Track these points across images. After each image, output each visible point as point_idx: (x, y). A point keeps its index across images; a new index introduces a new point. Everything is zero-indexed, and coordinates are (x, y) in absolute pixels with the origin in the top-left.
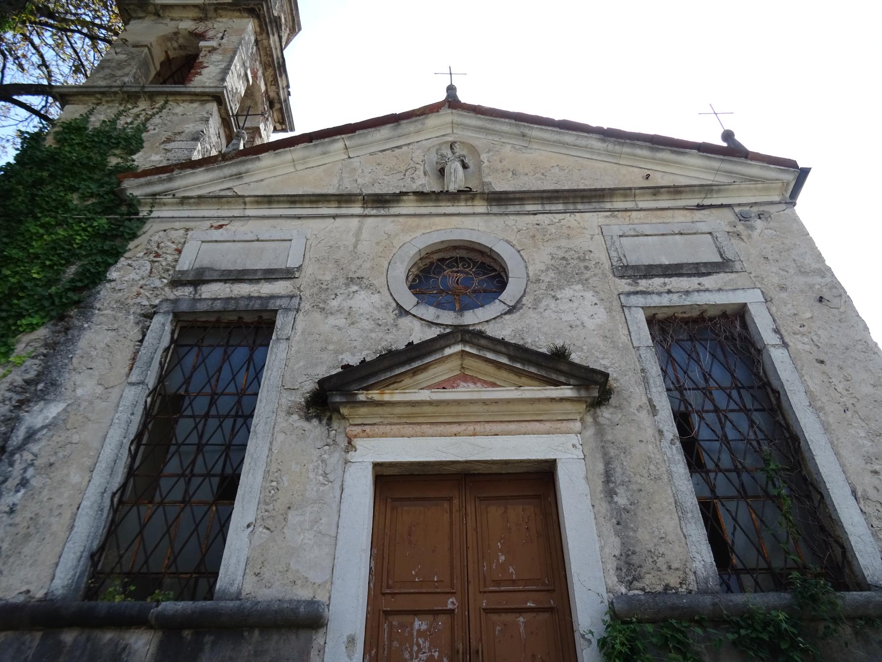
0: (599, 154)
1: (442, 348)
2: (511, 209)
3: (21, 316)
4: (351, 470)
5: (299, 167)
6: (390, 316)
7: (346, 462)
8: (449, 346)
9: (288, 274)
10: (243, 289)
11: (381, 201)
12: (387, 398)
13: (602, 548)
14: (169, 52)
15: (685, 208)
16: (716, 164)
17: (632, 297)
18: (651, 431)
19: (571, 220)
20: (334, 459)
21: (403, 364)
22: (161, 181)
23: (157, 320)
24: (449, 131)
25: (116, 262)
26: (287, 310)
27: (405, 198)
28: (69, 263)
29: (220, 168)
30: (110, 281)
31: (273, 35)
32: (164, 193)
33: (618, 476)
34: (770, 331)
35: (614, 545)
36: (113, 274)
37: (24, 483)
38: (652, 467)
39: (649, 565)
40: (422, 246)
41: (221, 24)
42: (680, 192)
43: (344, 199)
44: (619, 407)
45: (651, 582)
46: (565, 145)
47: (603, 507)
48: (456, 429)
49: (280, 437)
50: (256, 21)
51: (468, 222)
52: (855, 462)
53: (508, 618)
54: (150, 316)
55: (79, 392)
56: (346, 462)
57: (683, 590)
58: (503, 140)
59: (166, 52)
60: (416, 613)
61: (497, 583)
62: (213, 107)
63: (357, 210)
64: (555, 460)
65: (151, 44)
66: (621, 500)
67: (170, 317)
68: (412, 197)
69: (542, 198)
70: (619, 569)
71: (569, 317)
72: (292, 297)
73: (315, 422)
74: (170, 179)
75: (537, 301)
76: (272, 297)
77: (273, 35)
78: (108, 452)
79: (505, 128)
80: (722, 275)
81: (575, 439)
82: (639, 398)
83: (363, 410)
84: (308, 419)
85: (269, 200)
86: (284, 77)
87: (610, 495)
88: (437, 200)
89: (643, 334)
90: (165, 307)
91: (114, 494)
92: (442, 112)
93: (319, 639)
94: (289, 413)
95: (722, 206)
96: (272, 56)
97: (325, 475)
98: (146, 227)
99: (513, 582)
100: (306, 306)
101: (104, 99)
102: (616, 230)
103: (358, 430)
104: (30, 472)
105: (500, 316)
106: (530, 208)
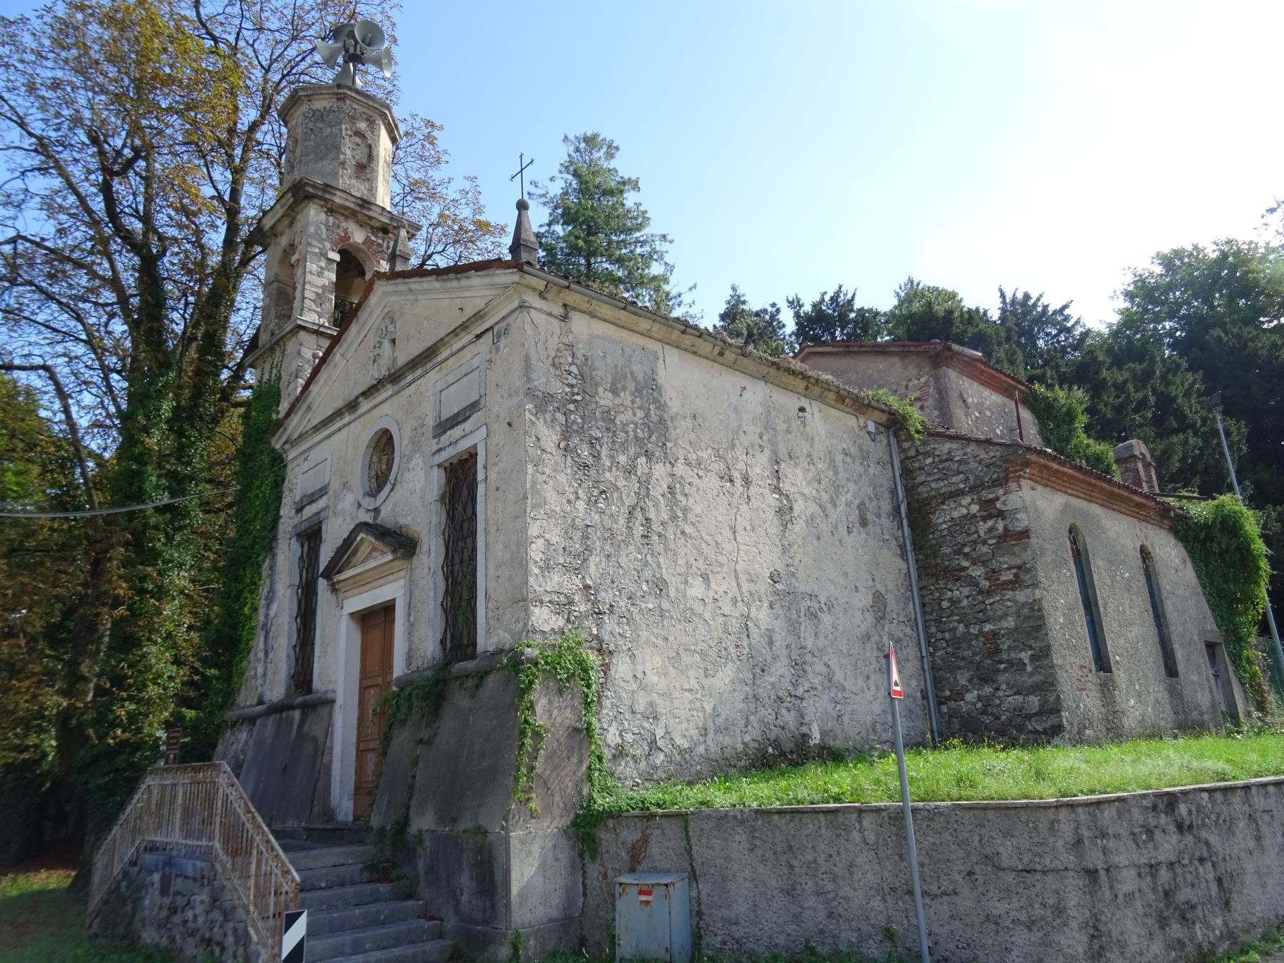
1: (355, 538)
2: (403, 383)
9: (323, 491)
11: (352, 406)
22: (283, 433)
24: (386, 300)
36: (282, 513)
42: (467, 327)
50: (316, 200)
62: (302, 334)
66: (412, 619)
74: (285, 429)
82: (425, 548)
86: (373, 207)
87: (409, 615)
88: (378, 390)
92: (375, 287)
106: (409, 378)
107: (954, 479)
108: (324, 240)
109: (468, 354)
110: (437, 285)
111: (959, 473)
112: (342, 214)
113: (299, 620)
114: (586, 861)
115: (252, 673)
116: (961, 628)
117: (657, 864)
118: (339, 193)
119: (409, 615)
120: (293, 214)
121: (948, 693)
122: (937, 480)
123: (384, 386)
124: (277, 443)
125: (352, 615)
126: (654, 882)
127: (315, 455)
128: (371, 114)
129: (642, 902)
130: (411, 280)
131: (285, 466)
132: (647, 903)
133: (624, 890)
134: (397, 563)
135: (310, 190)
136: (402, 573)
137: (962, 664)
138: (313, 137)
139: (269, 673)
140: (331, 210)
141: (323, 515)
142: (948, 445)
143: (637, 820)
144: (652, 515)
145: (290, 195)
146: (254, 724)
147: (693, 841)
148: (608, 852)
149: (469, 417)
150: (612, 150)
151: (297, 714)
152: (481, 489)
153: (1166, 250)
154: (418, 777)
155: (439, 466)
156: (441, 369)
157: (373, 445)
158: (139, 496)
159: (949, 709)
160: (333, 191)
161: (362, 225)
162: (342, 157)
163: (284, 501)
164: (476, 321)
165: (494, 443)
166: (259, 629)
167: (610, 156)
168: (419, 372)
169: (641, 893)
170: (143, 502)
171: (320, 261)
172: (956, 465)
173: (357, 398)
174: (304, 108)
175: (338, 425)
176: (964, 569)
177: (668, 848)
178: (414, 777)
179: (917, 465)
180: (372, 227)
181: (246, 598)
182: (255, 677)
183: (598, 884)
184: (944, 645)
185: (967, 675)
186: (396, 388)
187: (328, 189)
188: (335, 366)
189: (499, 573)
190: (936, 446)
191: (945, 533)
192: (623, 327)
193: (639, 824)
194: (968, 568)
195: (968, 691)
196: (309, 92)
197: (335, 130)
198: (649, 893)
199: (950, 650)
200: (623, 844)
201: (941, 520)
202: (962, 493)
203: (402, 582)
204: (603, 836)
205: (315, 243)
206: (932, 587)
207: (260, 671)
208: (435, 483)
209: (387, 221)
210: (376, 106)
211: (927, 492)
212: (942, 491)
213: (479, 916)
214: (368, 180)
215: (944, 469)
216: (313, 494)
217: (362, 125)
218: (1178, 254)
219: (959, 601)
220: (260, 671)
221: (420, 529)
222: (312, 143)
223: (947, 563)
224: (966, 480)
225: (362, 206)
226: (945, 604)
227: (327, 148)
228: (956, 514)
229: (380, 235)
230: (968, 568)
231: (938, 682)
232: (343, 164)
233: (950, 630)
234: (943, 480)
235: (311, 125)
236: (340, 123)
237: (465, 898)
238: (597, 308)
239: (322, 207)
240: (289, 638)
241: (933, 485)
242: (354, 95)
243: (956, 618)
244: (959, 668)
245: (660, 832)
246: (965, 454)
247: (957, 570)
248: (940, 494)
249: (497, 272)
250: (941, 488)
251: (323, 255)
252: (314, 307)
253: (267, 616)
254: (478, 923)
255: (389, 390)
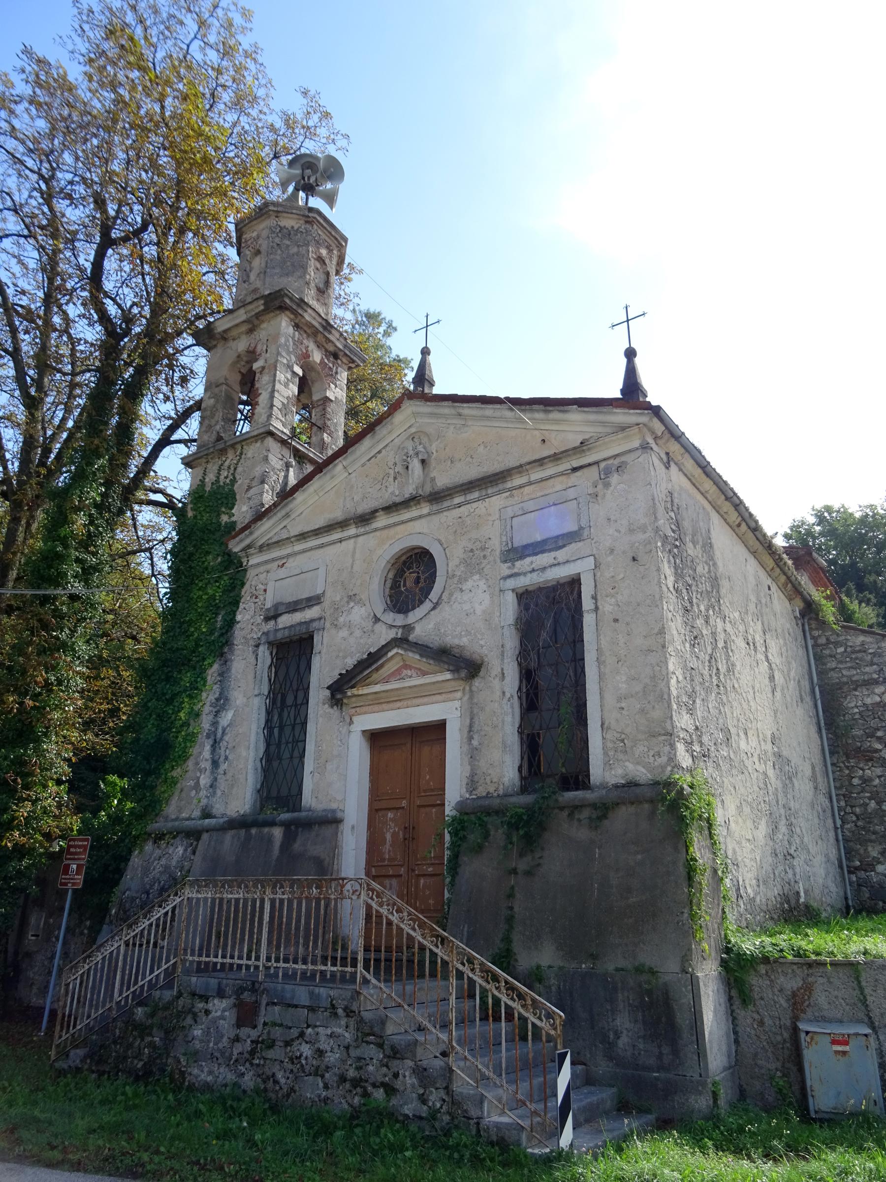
0: (512, 422)
1: (386, 653)
2: (446, 504)
3: (204, 659)
4: (352, 735)
5: (321, 494)
6: (368, 624)
7: (350, 732)
8: (390, 651)
9: (313, 601)
10: (298, 617)
11: (364, 519)
12: (360, 692)
13: (462, 773)
14: (242, 371)
15: (562, 474)
16: (592, 417)
17: (508, 580)
18: (498, 693)
19: (481, 507)
20: (344, 730)
21: (368, 667)
22: (247, 536)
23: (261, 648)
24: (413, 421)
25: (238, 608)
26: (319, 630)
27: (377, 514)
28: (217, 614)
29: (275, 514)
30: (239, 622)
31: (306, 311)
32: (249, 547)
33: (476, 727)
34: (589, 597)
35: (467, 772)
36: (239, 617)
37: (226, 758)
38: (495, 719)
39: (481, 781)
40: (388, 558)
41: (265, 330)
43: (342, 524)
44: (483, 678)
45: (481, 791)
46: (488, 418)
47: (466, 748)
48: (398, 704)
49: (321, 720)
50: (288, 313)
51: (418, 526)
52: (610, 700)
53: (428, 809)
54: (257, 646)
55: (238, 702)
56: (350, 732)
57: (495, 794)
58: (449, 422)
59: (240, 372)
60: (389, 809)
61: (425, 791)
62: (270, 441)
63: (352, 531)
64: (445, 720)
65: (226, 379)
66: (475, 743)
67: (267, 646)
68: (381, 513)
69: (464, 490)
70: (467, 784)
71: (466, 607)
72: (320, 619)
73: (335, 707)
74: (251, 533)
75: (451, 595)
76: (312, 621)
77: (306, 311)
78: (253, 738)
79: (446, 411)
80: (573, 545)
81: (457, 704)
82: (496, 671)
83: (354, 699)
84: (332, 707)
85: (303, 536)
86: (333, 331)
87: (470, 738)
89: (510, 608)
90: (263, 640)
91: (261, 759)
92: (403, 406)
93: (341, 827)
94: (324, 704)
95: (590, 465)
96: (314, 326)
97: (341, 741)
98: (248, 573)
99: (432, 790)
100: (328, 625)
101: (210, 457)
102: (510, 512)
103: (353, 710)
104: (228, 752)
105: (428, 613)
106: (457, 500)
107: (867, 669)
108: (291, 352)
109: (558, 484)
110: (508, 414)
111: (872, 664)
112: (305, 332)
113: (265, 731)
114: (735, 1007)
115: (192, 783)
116: (873, 804)
117: (825, 1013)
118: (310, 311)
119: (470, 738)
120: (256, 322)
121: (858, 863)
122: (852, 668)
123: (419, 503)
124: (235, 546)
125: (364, 732)
126: (851, 1031)
127: (293, 564)
128: (331, 242)
129: (837, 1052)
130: (465, 405)
131: (245, 570)
132: (844, 1053)
133: (812, 1039)
134: (453, 683)
135: (288, 301)
136: (459, 695)
137: (873, 837)
138: (279, 252)
139: (222, 784)
140: (297, 326)
141: (315, 625)
142: (861, 638)
143: (795, 967)
144: (720, 667)
145: (262, 302)
146: (198, 839)
147: (868, 991)
148: (762, 999)
149: (564, 546)
150: (391, 328)
151: (278, 833)
152: (588, 620)
153: (818, 506)
154: (516, 909)
155: (513, 590)
156: (512, 496)
157: (392, 562)
158: (58, 580)
159: (858, 878)
160: (305, 307)
161: (319, 346)
162: (308, 277)
163: (241, 606)
164: (574, 454)
165: (608, 574)
166: (201, 738)
167: (387, 334)
168: (476, 495)
169: (834, 1042)
170: (57, 585)
171: (287, 372)
172: (869, 657)
173: (376, 511)
174: (271, 222)
175: (336, 536)
176: (877, 751)
177: (836, 997)
178: (511, 908)
179: (827, 652)
180: (326, 350)
181: (183, 702)
182: (197, 787)
183: (753, 1032)
184: (854, 818)
185: (879, 848)
186: (435, 507)
187: (302, 304)
188: (332, 477)
189: (623, 705)
190: (849, 637)
191: (857, 716)
192: (694, 485)
193: (798, 971)
194: (881, 751)
195: (879, 863)
196: (280, 209)
197: (303, 250)
198: (846, 1043)
199: (860, 823)
200: (781, 991)
201: (853, 705)
202: (876, 682)
203: (457, 704)
204: (754, 982)
205: (284, 354)
206: (842, 765)
207: (204, 781)
208: (511, 608)
209: (341, 347)
210: (337, 237)
211: (838, 678)
212: (854, 679)
213: (652, 1061)
214: (326, 304)
215: (857, 658)
216: (296, 602)
217: (324, 252)
218: (828, 509)
219: (871, 780)
220: (204, 781)
221: (485, 651)
222: (278, 257)
223: (859, 744)
224: (879, 671)
225: (325, 328)
226: (856, 781)
227: (293, 265)
228: (868, 701)
229: (332, 359)
230: (881, 751)
231: (849, 852)
232: (308, 283)
233: (861, 805)
234: (855, 669)
235: (277, 240)
236: (307, 245)
237: (624, 1041)
238: (686, 463)
239: (291, 320)
240: (257, 749)
241: (844, 672)
242: (322, 221)
243: (867, 795)
244: (871, 841)
245: (825, 980)
246: (879, 648)
247: (868, 751)
248: (852, 681)
249: (615, 410)
250: (854, 675)
251: (290, 367)
252: (280, 416)
253: (215, 724)
254: (649, 1069)
255: (425, 509)
